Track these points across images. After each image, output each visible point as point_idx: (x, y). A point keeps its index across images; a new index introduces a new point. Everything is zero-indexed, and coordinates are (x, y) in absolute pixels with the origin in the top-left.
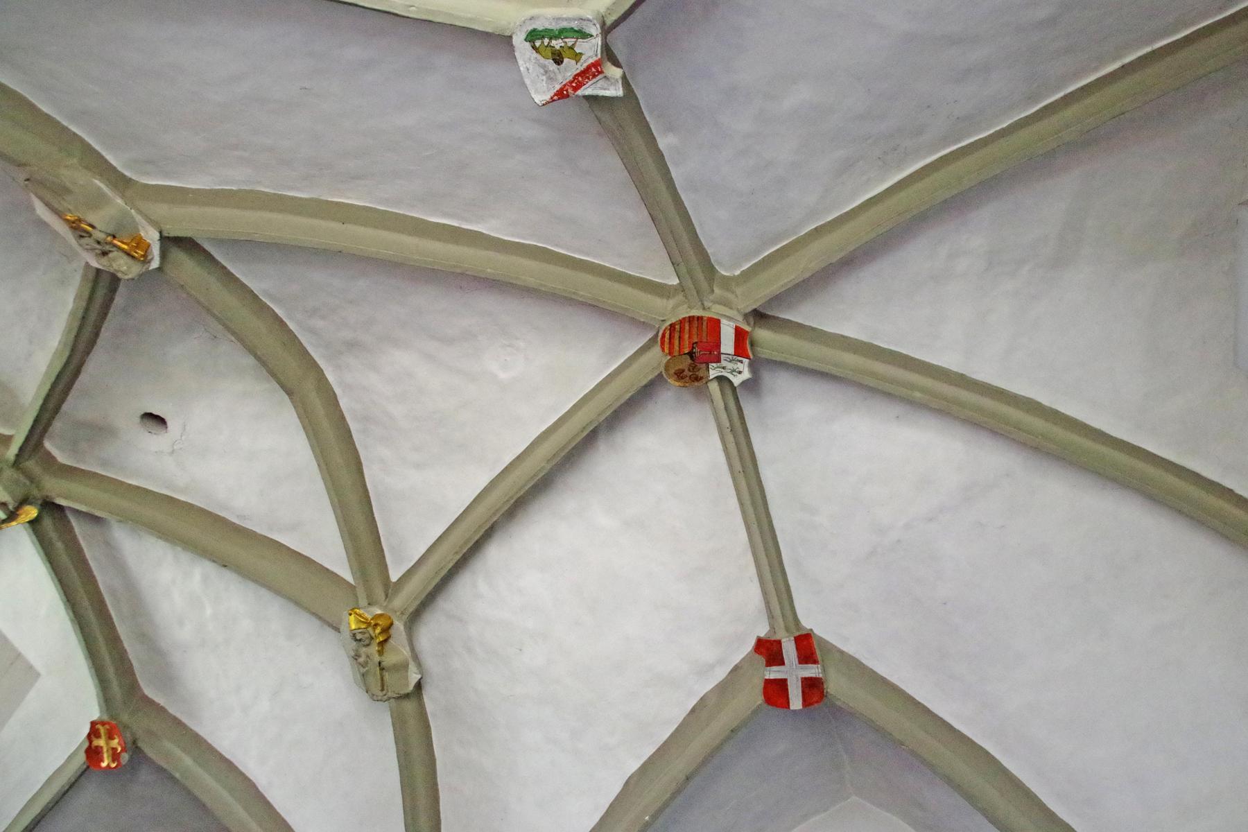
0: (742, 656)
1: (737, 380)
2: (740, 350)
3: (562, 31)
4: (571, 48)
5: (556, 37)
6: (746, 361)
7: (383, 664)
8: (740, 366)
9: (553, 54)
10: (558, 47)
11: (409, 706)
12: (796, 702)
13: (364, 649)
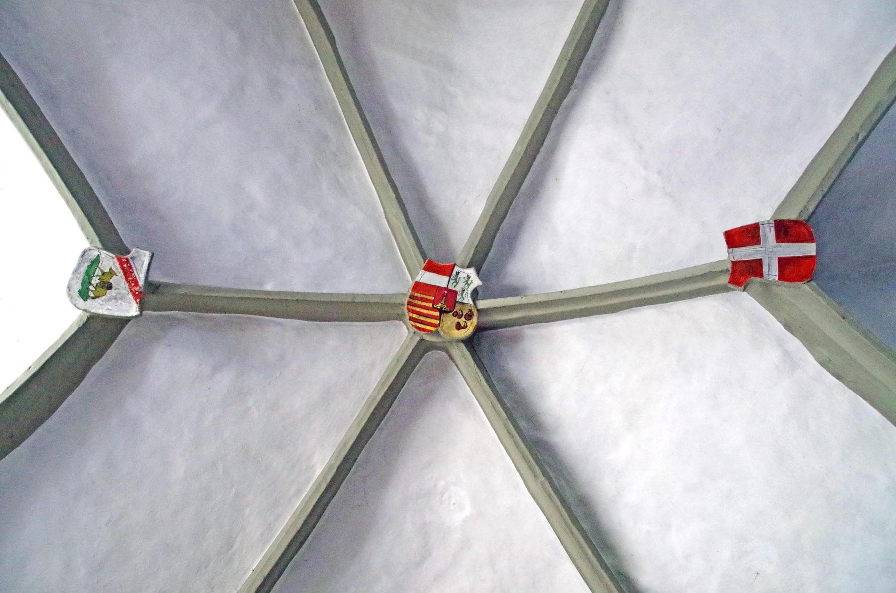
0: (775, 321)
1: (476, 282)
2: (446, 270)
4: (103, 273)
5: (90, 278)
9: (102, 287)
10: (98, 281)
12: (810, 249)
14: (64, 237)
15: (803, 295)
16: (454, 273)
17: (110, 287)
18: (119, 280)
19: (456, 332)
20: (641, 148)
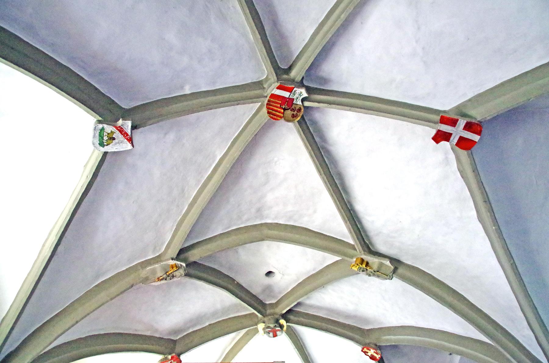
2: (290, 90)
3: (100, 136)
4: (108, 134)
6: (295, 89)
7: (375, 270)
11: (400, 270)
14: (82, 122)
17: (114, 139)
18: (117, 135)
20: (419, 28)
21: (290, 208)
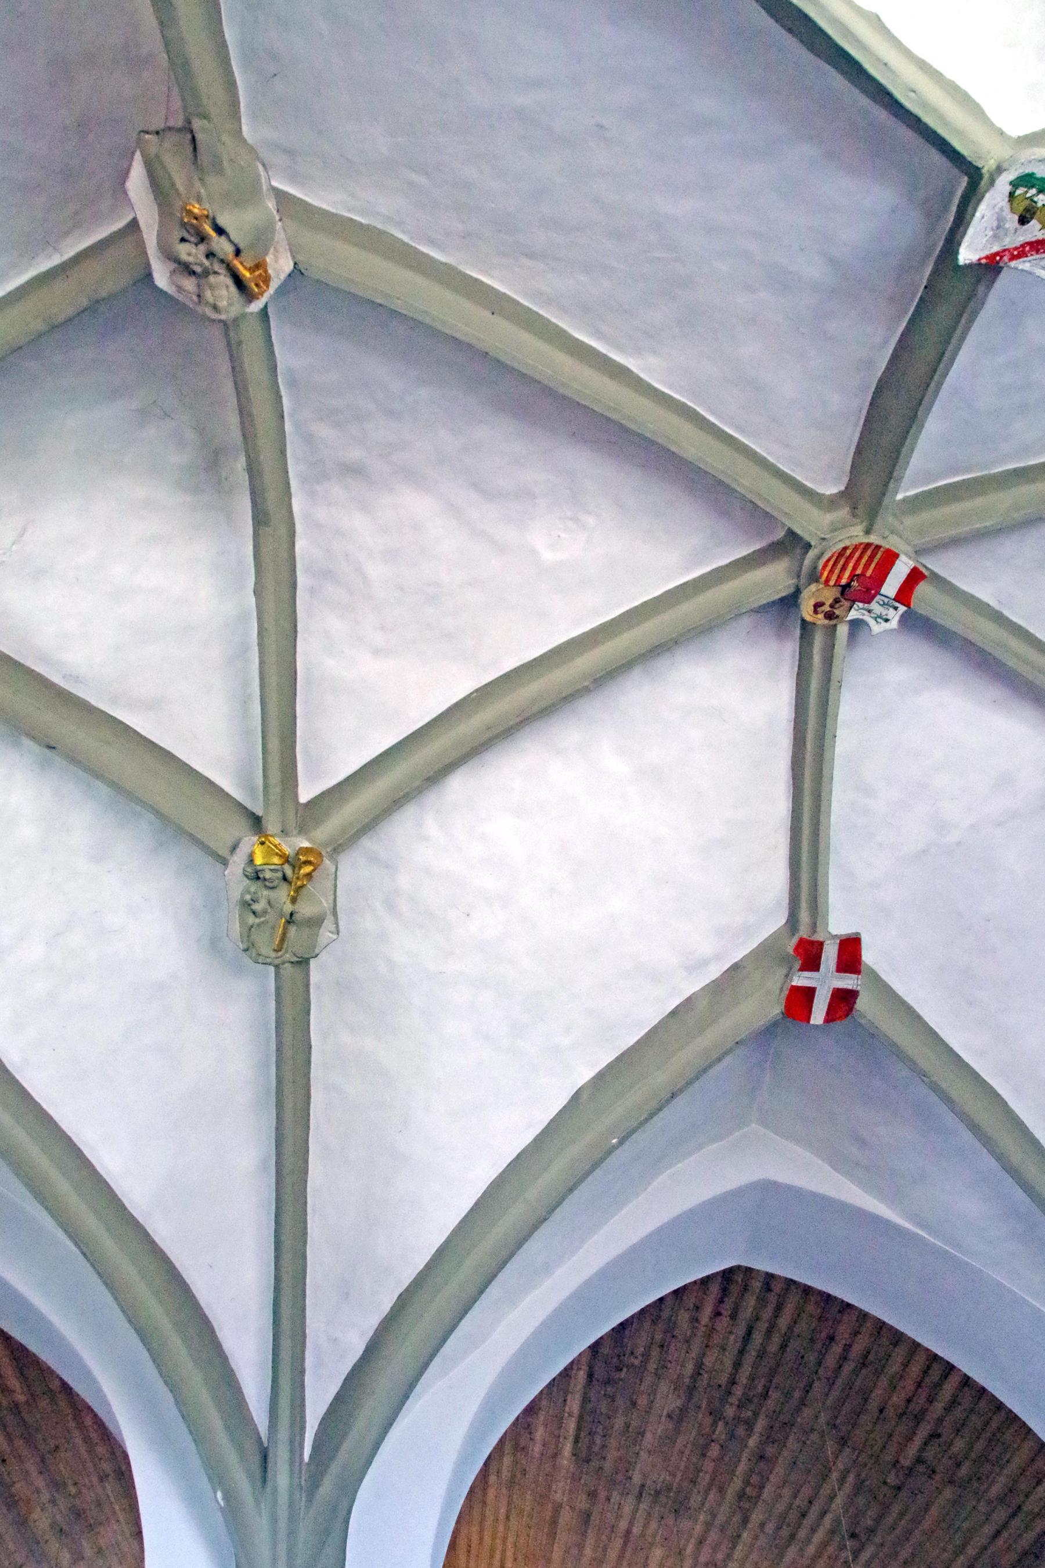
7: (296, 917)
8: (891, 613)
12: (818, 1016)
13: (266, 892)
15: (764, 1003)
16: (897, 604)
19: (812, 602)
21: (376, 571)
